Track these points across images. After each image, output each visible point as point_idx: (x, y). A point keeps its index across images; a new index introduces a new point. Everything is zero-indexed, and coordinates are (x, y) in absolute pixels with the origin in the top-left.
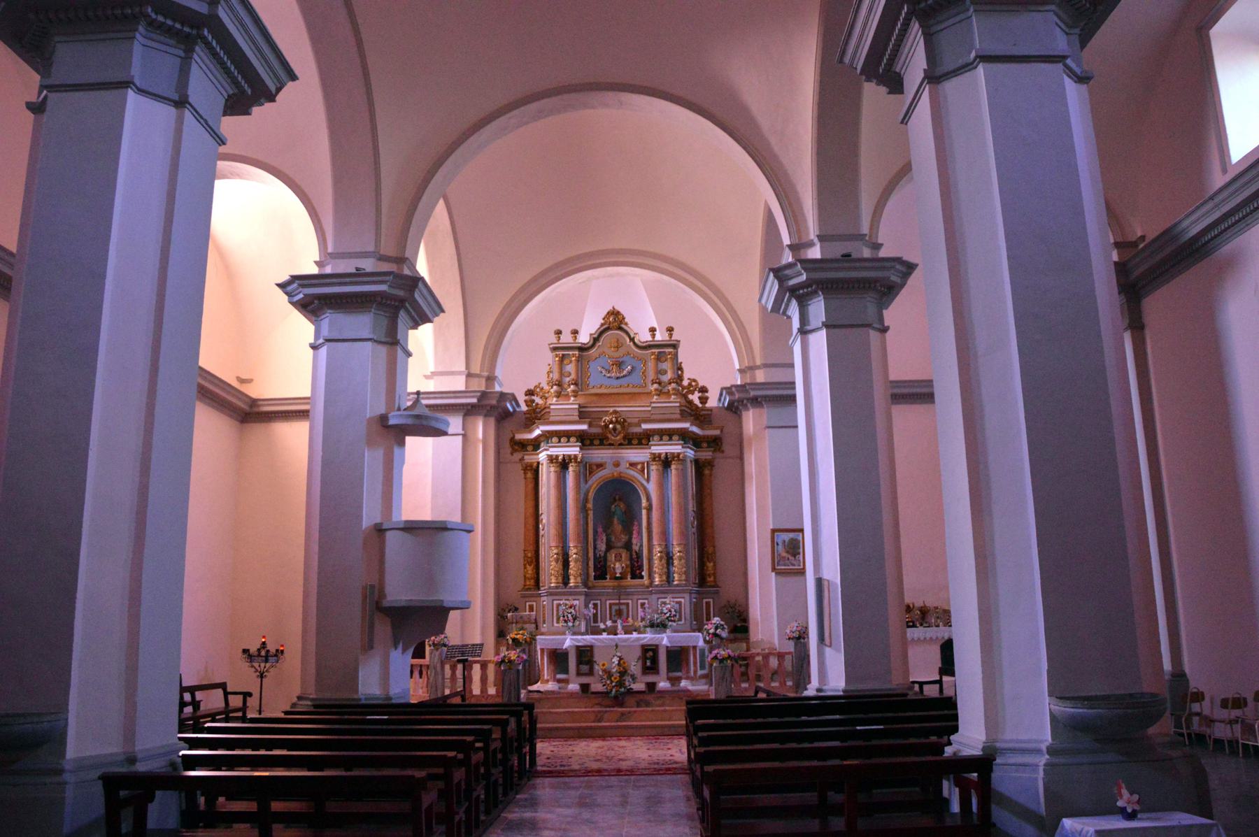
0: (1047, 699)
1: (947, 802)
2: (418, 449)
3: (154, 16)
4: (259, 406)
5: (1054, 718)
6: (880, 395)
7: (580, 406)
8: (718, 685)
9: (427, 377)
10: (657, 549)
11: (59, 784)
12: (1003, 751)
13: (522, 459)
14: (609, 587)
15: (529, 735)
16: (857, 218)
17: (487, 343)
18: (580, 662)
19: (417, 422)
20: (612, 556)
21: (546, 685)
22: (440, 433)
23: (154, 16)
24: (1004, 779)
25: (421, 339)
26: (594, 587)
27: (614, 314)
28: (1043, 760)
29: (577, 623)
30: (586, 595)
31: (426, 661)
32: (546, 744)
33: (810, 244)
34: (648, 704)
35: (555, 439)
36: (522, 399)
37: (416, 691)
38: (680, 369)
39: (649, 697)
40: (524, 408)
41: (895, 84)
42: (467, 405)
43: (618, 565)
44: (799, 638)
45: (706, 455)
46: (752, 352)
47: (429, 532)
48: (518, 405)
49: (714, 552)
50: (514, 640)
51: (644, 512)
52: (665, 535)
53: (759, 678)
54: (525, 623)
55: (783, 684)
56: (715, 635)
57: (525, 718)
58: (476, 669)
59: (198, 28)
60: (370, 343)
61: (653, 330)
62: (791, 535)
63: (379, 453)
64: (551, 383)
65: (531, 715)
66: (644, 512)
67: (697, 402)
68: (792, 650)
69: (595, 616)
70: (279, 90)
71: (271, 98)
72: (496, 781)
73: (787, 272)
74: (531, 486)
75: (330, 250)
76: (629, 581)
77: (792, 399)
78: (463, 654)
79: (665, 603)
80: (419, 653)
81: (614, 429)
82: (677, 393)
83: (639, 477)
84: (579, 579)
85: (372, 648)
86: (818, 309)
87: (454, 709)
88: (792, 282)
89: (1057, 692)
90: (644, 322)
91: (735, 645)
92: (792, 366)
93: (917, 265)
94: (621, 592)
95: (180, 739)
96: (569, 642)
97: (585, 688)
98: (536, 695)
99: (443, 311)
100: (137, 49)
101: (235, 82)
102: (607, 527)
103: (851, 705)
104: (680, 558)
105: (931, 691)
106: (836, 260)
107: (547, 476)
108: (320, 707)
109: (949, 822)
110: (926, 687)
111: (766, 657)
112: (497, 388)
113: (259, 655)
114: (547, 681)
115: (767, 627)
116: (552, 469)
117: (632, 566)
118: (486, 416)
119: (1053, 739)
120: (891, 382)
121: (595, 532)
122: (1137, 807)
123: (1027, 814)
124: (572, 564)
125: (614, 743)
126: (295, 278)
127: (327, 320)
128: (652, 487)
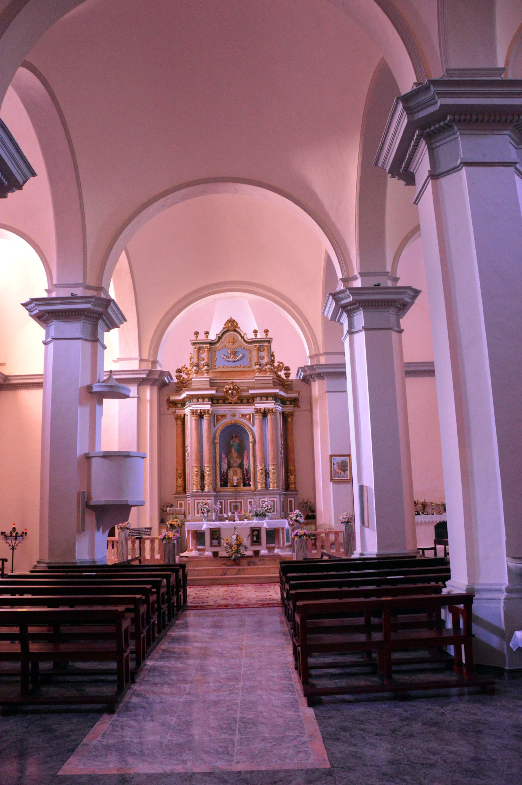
0: (506, 559)
1: (444, 622)
2: (111, 407)
4: (9, 380)
5: (510, 571)
7: (210, 380)
8: (298, 551)
9: (114, 361)
12: (479, 591)
13: (175, 412)
15: (183, 584)
16: (384, 264)
17: (152, 341)
18: (212, 538)
19: (111, 390)
20: (231, 473)
21: (191, 553)
22: (126, 396)
24: (479, 608)
25: (111, 338)
27: (231, 321)
28: (504, 595)
29: (210, 514)
31: (116, 538)
32: (192, 589)
33: (355, 278)
34: (255, 564)
35: (195, 400)
36: (174, 374)
37: (109, 557)
38: (273, 356)
39: (256, 560)
40: (175, 380)
41: (410, 179)
42: (140, 378)
43: (235, 478)
44: (348, 522)
45: (289, 409)
48: (172, 379)
49: (294, 470)
50: (171, 525)
51: (251, 445)
52: (264, 458)
53: (323, 547)
54: (178, 514)
55: (338, 550)
57: (180, 573)
58: (148, 543)
60: (80, 341)
61: (255, 332)
62: (342, 459)
63: (87, 409)
64: (192, 365)
65: (184, 572)
66: (251, 445)
67: (283, 376)
68: (344, 529)
69: (221, 510)
70: (24, 182)
71: (20, 187)
72: (164, 612)
73: (341, 296)
74: (180, 429)
75: (55, 282)
77: (344, 374)
78: (139, 534)
79: (264, 501)
80: (112, 534)
81: (232, 393)
82: (271, 371)
86: (360, 318)
87: (135, 568)
88: (343, 302)
89: (512, 554)
90: (249, 327)
91: (308, 527)
92: (343, 354)
93: (421, 291)
94: (237, 495)
96: (205, 526)
97: (215, 554)
98: (185, 559)
99: (126, 321)
102: (228, 454)
103: (382, 563)
104: (274, 473)
105: (430, 554)
107: (190, 422)
108: (52, 568)
109: (445, 635)
110: (426, 552)
111: (327, 534)
112: (159, 368)
113: (11, 536)
114: (192, 550)
115: (328, 516)
116: (194, 418)
117: (244, 479)
118: (151, 385)
119: (509, 583)
120: (405, 363)
124: (206, 478)
126: (33, 300)
127: (53, 327)
128: (256, 429)
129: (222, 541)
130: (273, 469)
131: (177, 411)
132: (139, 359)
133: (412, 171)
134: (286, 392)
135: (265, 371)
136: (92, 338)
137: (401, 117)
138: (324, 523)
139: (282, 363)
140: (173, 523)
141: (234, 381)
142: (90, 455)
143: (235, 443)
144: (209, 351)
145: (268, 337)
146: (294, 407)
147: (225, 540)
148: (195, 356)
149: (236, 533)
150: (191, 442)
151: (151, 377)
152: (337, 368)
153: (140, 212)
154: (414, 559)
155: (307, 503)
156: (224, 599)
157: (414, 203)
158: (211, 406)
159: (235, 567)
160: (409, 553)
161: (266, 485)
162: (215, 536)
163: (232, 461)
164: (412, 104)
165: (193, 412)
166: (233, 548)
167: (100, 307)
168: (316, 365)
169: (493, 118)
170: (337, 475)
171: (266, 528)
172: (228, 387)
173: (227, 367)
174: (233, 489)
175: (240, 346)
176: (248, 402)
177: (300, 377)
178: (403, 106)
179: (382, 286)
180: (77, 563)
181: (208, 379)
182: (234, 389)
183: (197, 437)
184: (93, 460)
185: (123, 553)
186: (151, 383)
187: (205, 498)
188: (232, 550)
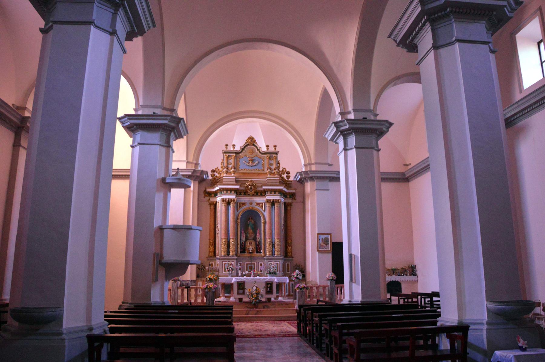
0: (486, 302)
2: (176, 194)
6: (377, 178)
10: (268, 241)
11: (62, 339)
13: (210, 199)
14: (247, 256)
18: (239, 288)
20: (248, 243)
24: (471, 336)
25: (179, 146)
28: (485, 327)
30: (237, 259)
33: (349, 113)
34: (268, 307)
35: (225, 192)
36: (210, 173)
38: (279, 163)
42: (187, 175)
43: (250, 247)
45: (289, 201)
46: (310, 158)
47: (181, 230)
48: (208, 176)
50: (210, 278)
51: (262, 225)
52: (271, 234)
56: (297, 278)
58: (193, 292)
60: (158, 146)
61: (234, 146)
62: (325, 236)
66: (262, 225)
67: (285, 178)
68: (329, 284)
73: (341, 124)
75: (141, 104)
76: (255, 254)
77: (338, 179)
81: (251, 188)
84: (234, 253)
85: (157, 280)
88: (342, 128)
94: (252, 259)
100: (95, 7)
101: (131, 26)
103: (363, 307)
107: (221, 208)
116: (223, 205)
117: (257, 248)
121: (241, 232)
122: (527, 346)
123: (477, 349)
124: (231, 246)
125: (260, 324)
126: (126, 115)
128: (266, 214)
129: (246, 291)
133: (415, 43)
134: (287, 189)
135: (274, 174)
137: (416, 7)
142: (163, 227)
143: (251, 223)
151: (194, 174)
153: (201, 59)
165: (223, 200)
169: (476, 12)
175: (257, 156)
176: (261, 195)
179: (368, 119)
182: (252, 185)
184: (165, 230)
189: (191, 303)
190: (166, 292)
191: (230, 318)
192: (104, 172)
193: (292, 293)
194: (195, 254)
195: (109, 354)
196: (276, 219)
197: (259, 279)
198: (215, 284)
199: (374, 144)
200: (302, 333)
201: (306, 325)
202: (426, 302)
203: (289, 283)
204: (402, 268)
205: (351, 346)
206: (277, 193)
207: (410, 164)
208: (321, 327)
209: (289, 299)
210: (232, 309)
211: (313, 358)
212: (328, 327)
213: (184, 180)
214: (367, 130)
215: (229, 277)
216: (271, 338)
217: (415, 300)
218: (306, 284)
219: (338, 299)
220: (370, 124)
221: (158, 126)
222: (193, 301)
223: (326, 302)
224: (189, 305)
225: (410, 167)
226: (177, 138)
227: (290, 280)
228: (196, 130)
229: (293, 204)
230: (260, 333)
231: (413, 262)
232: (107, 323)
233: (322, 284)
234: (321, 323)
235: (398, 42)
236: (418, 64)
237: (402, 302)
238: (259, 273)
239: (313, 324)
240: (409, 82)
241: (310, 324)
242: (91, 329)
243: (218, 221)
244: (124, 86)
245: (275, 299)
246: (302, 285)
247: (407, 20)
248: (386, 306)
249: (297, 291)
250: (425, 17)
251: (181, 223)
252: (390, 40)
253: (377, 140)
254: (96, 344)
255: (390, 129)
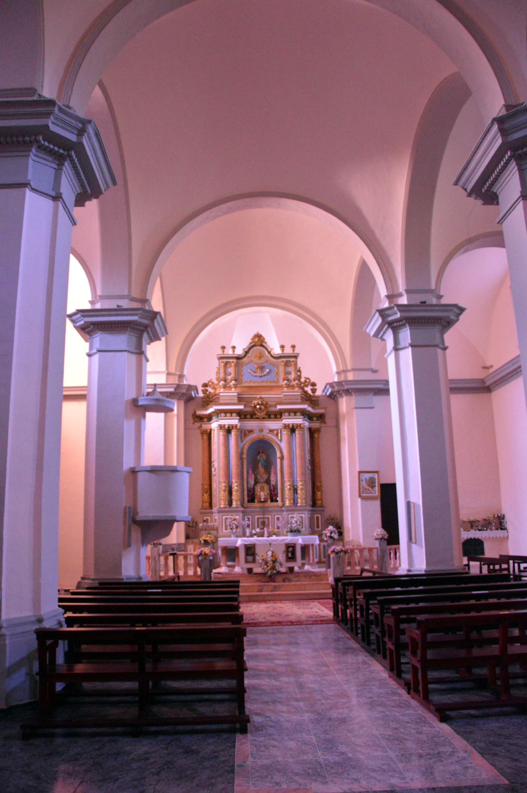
2: (154, 421)
3: (43, 142)
7: (239, 394)
8: (335, 567)
10: (287, 485)
13: (201, 426)
14: (257, 507)
16: (429, 280)
19: (157, 403)
20: (258, 488)
23: (43, 142)
25: (155, 351)
26: (247, 508)
27: (259, 336)
30: (243, 512)
33: (400, 295)
34: (290, 581)
35: (223, 415)
36: (200, 389)
38: (299, 371)
39: (290, 576)
40: (201, 394)
42: (167, 392)
43: (262, 494)
45: (316, 425)
48: (198, 393)
49: (321, 486)
50: (205, 541)
51: (278, 461)
52: (292, 474)
54: (211, 530)
56: (331, 537)
58: (181, 560)
59: (68, 151)
60: (126, 353)
61: (234, 348)
62: (370, 475)
64: (219, 380)
66: (278, 461)
67: (310, 392)
73: (387, 312)
74: (206, 444)
75: (99, 293)
77: (385, 391)
78: (173, 550)
79: (293, 517)
81: (260, 408)
83: (274, 438)
84: (239, 503)
85: (129, 546)
86: (406, 334)
94: (264, 510)
95: (60, 606)
100: (31, 162)
101: (82, 186)
103: (429, 579)
106: (417, 306)
107: (217, 438)
116: (221, 433)
117: (271, 494)
118: (179, 399)
121: (248, 473)
124: (234, 493)
125: (279, 605)
126: (79, 311)
128: (284, 445)
129: (257, 558)
130: (302, 485)
131: (203, 426)
132: (167, 372)
133: (495, 191)
134: (313, 408)
135: (293, 387)
136: (137, 351)
137: (494, 138)
138: (352, 540)
139: (308, 379)
140: (207, 539)
141: (263, 396)
143: (262, 458)
144: (235, 365)
145: (225, 353)
146: (320, 423)
147: (261, 556)
148: (222, 370)
149: (271, 549)
150: (219, 457)
151: (177, 392)
152: (367, 384)
154: (467, 575)
155: (333, 519)
156: (272, 616)
157: (498, 223)
158: (240, 421)
159: (270, 584)
160: (456, 570)
161: (294, 501)
162: (250, 552)
163: (258, 477)
164: (507, 125)
165: (221, 427)
166: (268, 564)
167: (147, 319)
168: (344, 381)
170: (365, 492)
171: (301, 545)
172: (256, 402)
173: (253, 382)
174: (261, 505)
175: (267, 361)
176: (276, 417)
177: (326, 393)
178: (498, 128)
180: (123, 579)
181: (236, 394)
182: (262, 404)
183: (224, 453)
185: (155, 569)
186: (178, 397)
187: (233, 514)
188: (268, 566)
189: (179, 577)
190: (143, 562)
191: (236, 600)
192: (51, 393)
193: (323, 559)
194: (182, 507)
195: (66, 654)
196: (297, 452)
197: (275, 541)
198: (213, 548)
199: (438, 341)
200: (340, 619)
201: (346, 607)
202: (522, 568)
203: (319, 545)
204: (485, 520)
205: (412, 639)
206: (298, 414)
207: (492, 366)
208: (368, 609)
209: (319, 567)
210: (238, 586)
211: (357, 655)
212: (378, 611)
213: (163, 400)
214: (427, 320)
215: (233, 538)
216: (297, 626)
217: (504, 566)
218: (343, 546)
219: (392, 566)
220: (431, 311)
221: (126, 325)
222: (181, 573)
223: (374, 573)
224: (176, 580)
225: (491, 370)
226: (152, 341)
227: (321, 540)
228: (178, 328)
229: (323, 430)
230: (280, 620)
231: (500, 509)
232: (62, 611)
233: (367, 546)
234: (368, 604)
235: (469, 190)
236: (500, 222)
237: (485, 571)
238: (276, 530)
239: (356, 605)
240: (486, 246)
241: (351, 605)
242: (40, 620)
243: (215, 457)
244: (75, 268)
245: (300, 568)
246: (338, 548)
247: (481, 159)
248: (461, 578)
249: (332, 556)
250: (509, 153)
251: (161, 463)
252: (458, 188)
253: (442, 333)
254: (49, 642)
255: (461, 317)
